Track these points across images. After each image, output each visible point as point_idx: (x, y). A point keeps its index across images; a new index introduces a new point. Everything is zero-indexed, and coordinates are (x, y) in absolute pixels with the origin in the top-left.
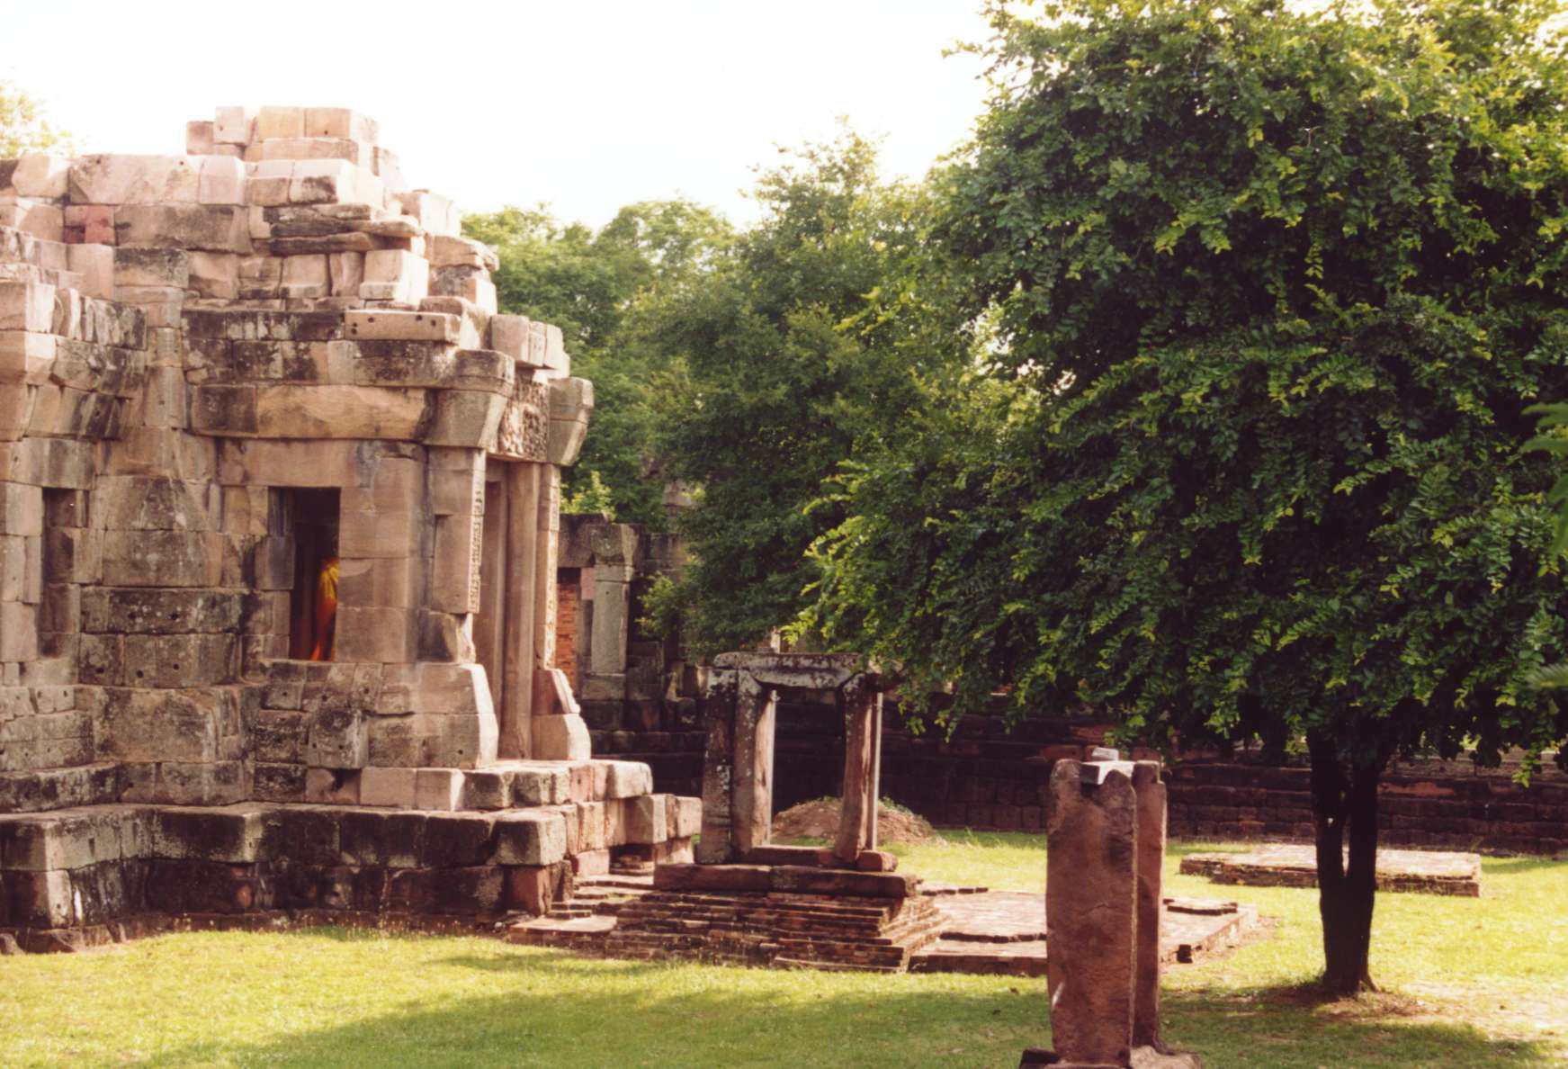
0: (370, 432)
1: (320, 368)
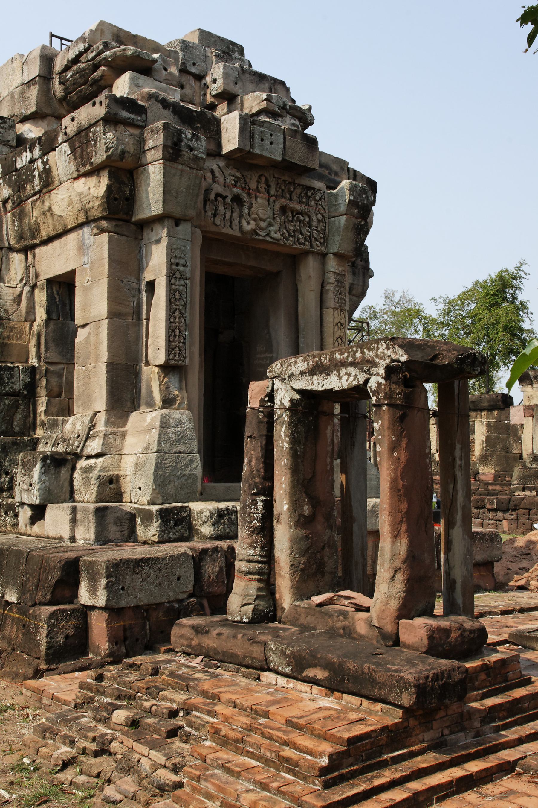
0: (82, 219)
1: (55, 173)
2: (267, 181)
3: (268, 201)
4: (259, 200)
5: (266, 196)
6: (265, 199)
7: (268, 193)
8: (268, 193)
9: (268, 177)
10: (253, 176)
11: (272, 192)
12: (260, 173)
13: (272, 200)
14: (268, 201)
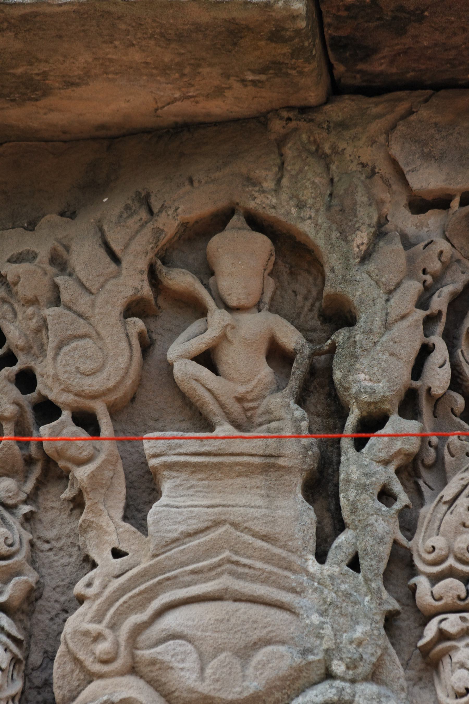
2: (292, 253)
3: (321, 485)
4: (177, 506)
5: (289, 426)
6: (269, 466)
7: (319, 389)
8: (319, 389)
9: (311, 227)
10: (85, 256)
11: (371, 373)
12: (194, 204)
13: (362, 469)
14: (321, 485)
